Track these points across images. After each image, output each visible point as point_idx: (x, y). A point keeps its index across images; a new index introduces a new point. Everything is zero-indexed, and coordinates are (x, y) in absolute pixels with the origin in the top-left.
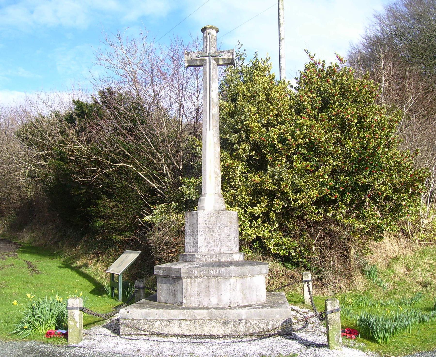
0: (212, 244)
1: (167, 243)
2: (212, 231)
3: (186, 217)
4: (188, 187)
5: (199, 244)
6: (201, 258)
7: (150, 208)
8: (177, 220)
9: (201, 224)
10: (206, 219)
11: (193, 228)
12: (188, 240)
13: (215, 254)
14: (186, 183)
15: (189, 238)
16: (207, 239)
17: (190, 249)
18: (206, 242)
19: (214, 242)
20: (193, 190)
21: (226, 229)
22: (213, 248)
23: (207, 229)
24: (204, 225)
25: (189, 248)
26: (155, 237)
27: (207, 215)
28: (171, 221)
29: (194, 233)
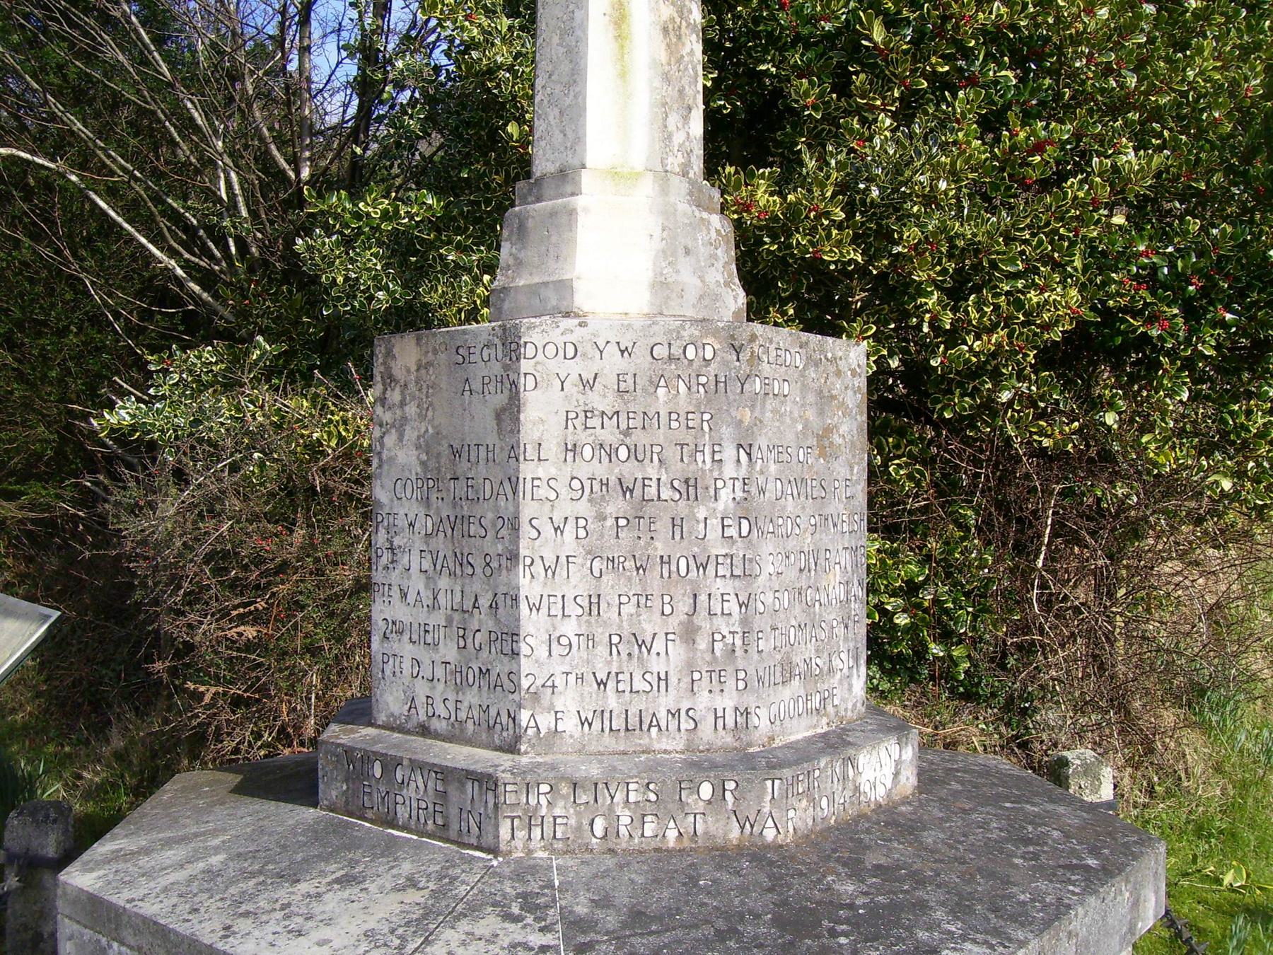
0: (669, 657)
1: (220, 560)
2: (663, 526)
3: (389, 379)
4: (348, 243)
5: (535, 662)
6: (562, 813)
7: (142, 365)
8: (278, 426)
9: (552, 450)
10: (602, 400)
11: (460, 488)
12: (407, 600)
13: (701, 764)
14: (336, 217)
15: (417, 584)
16: (610, 614)
17: (421, 689)
18: (601, 635)
19: (689, 633)
20: (372, 259)
21: (790, 505)
22: (665, 702)
23: (616, 506)
24: (591, 467)
25: (409, 666)
26: (159, 519)
27: (613, 363)
28: (247, 433)
29: (480, 530)
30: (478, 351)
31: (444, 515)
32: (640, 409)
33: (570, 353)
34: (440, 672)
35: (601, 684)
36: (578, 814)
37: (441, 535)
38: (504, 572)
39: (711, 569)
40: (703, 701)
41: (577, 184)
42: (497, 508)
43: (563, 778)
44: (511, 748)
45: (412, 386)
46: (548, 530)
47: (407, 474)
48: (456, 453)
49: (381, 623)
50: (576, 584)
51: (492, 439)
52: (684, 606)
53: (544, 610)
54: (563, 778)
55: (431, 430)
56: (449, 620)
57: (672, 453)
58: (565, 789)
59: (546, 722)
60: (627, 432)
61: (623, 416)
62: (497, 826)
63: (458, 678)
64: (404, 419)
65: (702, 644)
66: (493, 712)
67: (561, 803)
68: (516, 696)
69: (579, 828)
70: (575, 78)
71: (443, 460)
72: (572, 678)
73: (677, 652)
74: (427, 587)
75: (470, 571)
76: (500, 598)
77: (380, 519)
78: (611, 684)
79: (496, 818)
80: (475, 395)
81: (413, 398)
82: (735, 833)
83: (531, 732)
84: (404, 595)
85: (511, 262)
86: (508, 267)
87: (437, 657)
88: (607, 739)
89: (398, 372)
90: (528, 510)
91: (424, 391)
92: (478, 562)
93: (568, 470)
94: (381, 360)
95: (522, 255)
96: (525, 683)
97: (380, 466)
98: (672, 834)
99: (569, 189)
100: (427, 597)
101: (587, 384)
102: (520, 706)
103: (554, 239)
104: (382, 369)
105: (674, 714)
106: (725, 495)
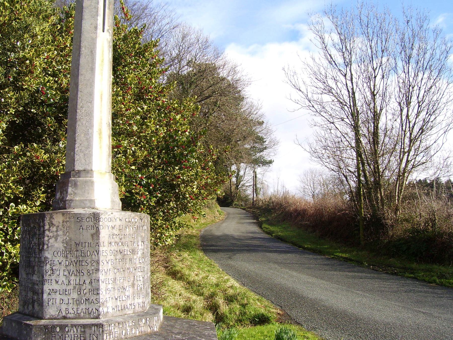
0: (129, 291)
2: (128, 261)
5: (104, 295)
9: (106, 244)
10: (116, 232)
11: (79, 253)
15: (62, 278)
16: (118, 282)
17: (64, 307)
18: (116, 288)
22: (129, 302)
23: (119, 256)
30: (85, 219)
31: (73, 260)
32: (123, 234)
33: (110, 220)
34: (71, 301)
35: (116, 299)
36: (120, 330)
37: (72, 265)
38: (94, 274)
39: (137, 270)
40: (136, 301)
41: (93, 175)
42: (92, 258)
43: (117, 322)
44: (97, 317)
45: (61, 227)
46: (105, 263)
47: (59, 250)
48: (77, 244)
49: (47, 290)
50: (111, 276)
51: (90, 241)
52: (132, 279)
53: (105, 282)
54: (117, 322)
55: (68, 238)
56: (75, 288)
57: (129, 244)
58: (117, 324)
59: (105, 310)
60: (121, 239)
61: (120, 235)
62: (103, 336)
63: (78, 302)
64: (58, 235)
65: (136, 288)
66: (90, 309)
67: (116, 328)
68: (98, 304)
69: (120, 334)
70: (89, 146)
71: (72, 246)
72: (110, 298)
73: (131, 290)
74: (66, 279)
75: (82, 274)
76: (93, 281)
77: (47, 262)
78: (118, 299)
79: (103, 334)
80: (84, 230)
81: (61, 230)
82: (149, 330)
83: (102, 313)
84: (57, 282)
85: (72, 193)
86: (71, 194)
87: (70, 298)
88: (118, 312)
89: (55, 222)
90: (101, 258)
91: (65, 228)
92: (85, 272)
93: (109, 249)
94: (48, 219)
95: (76, 191)
96: (101, 301)
97: (48, 248)
98: (138, 332)
99: (90, 176)
100: (66, 282)
101: (113, 228)
102: (100, 307)
103: (87, 188)
104: (49, 221)
105: (131, 305)
106: (140, 253)
